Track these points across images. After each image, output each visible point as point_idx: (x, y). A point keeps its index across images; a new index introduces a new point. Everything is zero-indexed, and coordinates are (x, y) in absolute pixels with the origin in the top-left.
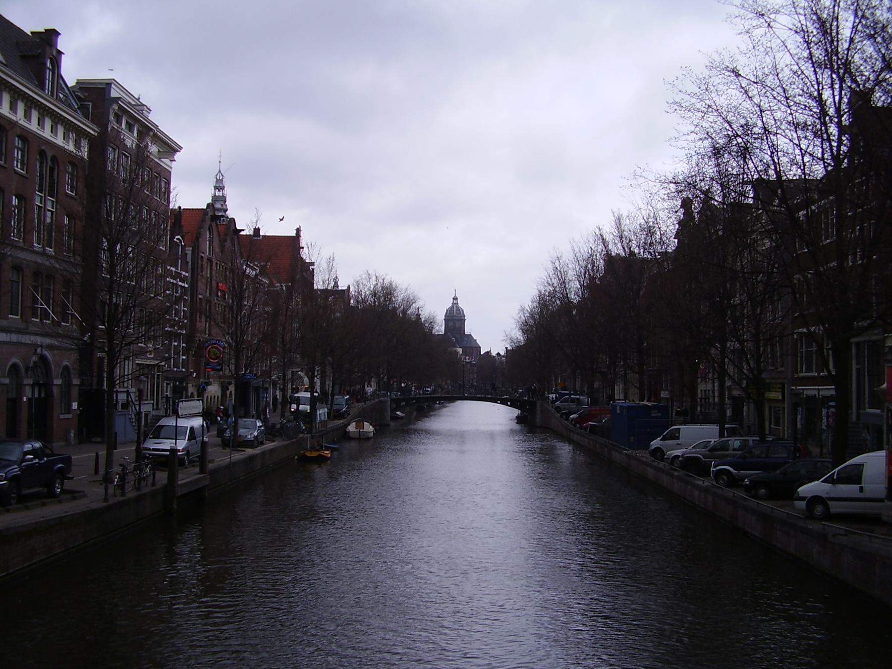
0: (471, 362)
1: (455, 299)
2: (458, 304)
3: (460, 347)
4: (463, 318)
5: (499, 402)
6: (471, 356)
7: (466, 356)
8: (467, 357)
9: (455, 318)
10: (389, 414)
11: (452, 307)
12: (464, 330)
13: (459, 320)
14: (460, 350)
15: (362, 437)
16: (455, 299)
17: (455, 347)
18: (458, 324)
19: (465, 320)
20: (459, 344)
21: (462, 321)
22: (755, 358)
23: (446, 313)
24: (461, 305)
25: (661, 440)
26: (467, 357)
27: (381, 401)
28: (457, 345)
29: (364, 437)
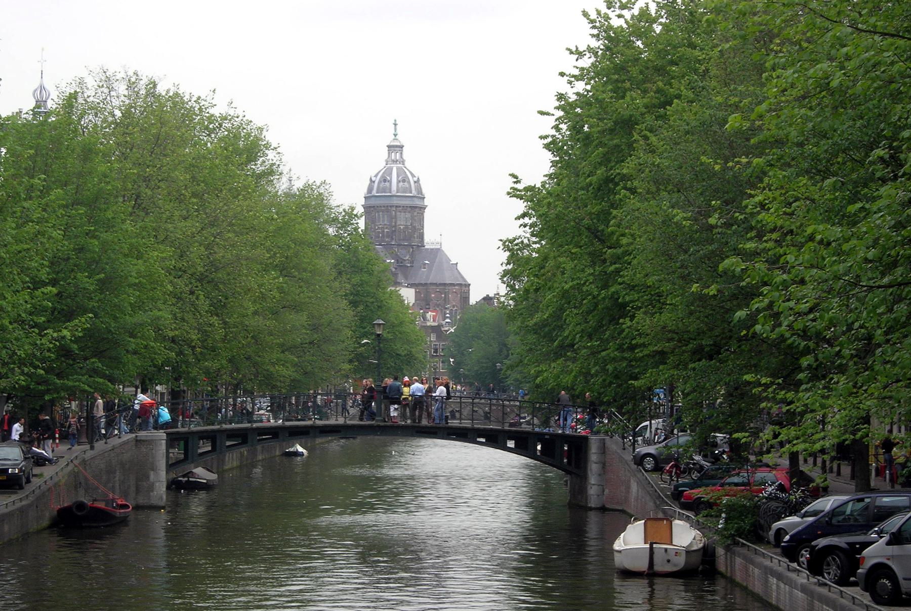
0: (440, 326)
1: (395, 148)
2: (403, 162)
3: (411, 286)
4: (417, 202)
5: (511, 444)
6: (441, 308)
7: (428, 309)
8: (430, 315)
9: (395, 202)
10: (163, 474)
11: (389, 171)
12: (421, 236)
13: (405, 208)
14: (408, 295)
15: (658, 568)
16: (395, 148)
17: (397, 284)
18: (402, 220)
19: (423, 208)
20: (406, 278)
21: (417, 210)
22: (151, 420)
23: (370, 190)
24: (414, 163)
25: (889, 543)
26: (430, 315)
27: (138, 441)
28: (401, 279)
29: (669, 568)
